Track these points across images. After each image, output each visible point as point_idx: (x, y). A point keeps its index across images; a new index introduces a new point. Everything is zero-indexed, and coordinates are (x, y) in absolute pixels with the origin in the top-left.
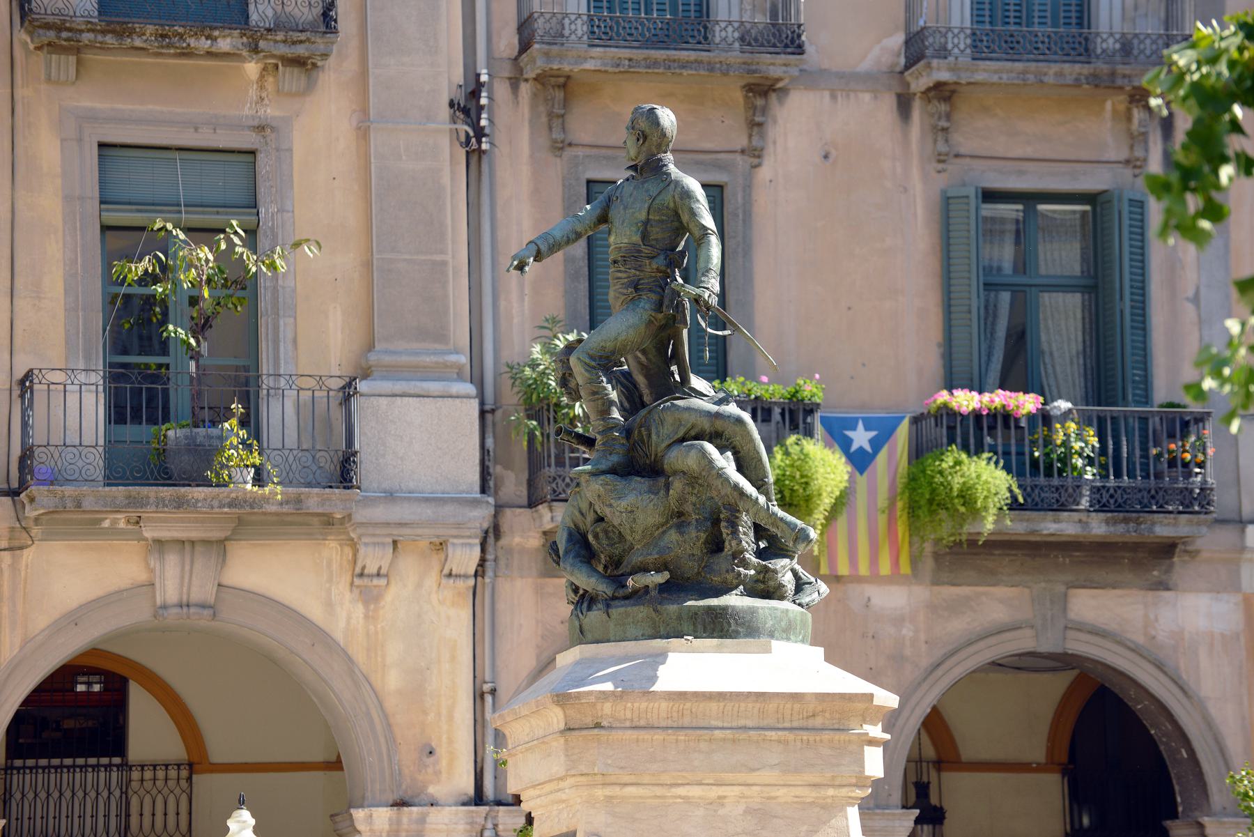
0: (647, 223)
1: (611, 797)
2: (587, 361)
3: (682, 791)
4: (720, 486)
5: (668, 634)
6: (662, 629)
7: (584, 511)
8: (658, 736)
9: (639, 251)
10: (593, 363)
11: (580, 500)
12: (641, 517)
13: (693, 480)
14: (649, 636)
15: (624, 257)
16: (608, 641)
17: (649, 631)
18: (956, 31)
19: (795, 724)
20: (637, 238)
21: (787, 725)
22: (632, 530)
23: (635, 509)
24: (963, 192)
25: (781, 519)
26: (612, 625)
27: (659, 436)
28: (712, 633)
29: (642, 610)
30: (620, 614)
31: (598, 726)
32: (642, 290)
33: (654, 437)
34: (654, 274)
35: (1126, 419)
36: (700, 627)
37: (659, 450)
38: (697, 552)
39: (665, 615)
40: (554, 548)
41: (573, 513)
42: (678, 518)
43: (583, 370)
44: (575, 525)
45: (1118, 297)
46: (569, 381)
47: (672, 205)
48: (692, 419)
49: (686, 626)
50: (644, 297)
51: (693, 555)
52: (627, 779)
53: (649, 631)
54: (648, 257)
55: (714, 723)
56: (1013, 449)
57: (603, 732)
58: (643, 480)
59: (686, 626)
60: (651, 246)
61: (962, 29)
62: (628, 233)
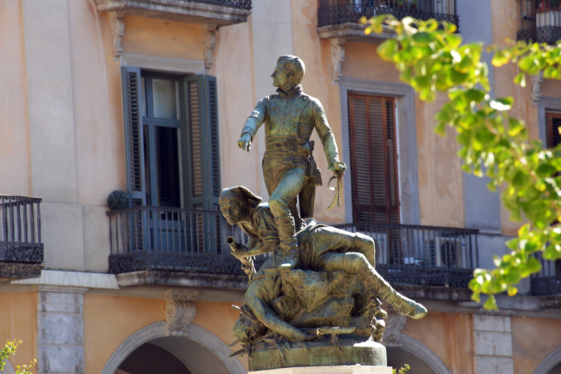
0: (299, 124)
2: (283, 203)
4: (372, 279)
5: (346, 363)
6: (343, 360)
7: (268, 289)
9: (296, 140)
10: (286, 205)
11: (265, 283)
12: (318, 295)
14: (335, 363)
15: (285, 143)
16: (308, 366)
17: (336, 361)
20: (294, 133)
23: (315, 290)
25: (403, 299)
26: (311, 357)
27: (316, 248)
28: (367, 363)
29: (331, 348)
30: (317, 350)
32: (298, 162)
33: (314, 248)
34: (302, 154)
36: (362, 359)
37: (317, 255)
39: (345, 352)
40: (117, 297)
41: (260, 289)
42: (333, 296)
43: (281, 209)
44: (263, 297)
46: (233, 212)
47: (311, 115)
48: (340, 239)
49: (356, 359)
50: (300, 167)
51: (346, 317)
53: (336, 361)
54: (299, 144)
56: (179, 229)
58: (316, 273)
59: (356, 359)
60: (301, 138)
62: (289, 129)
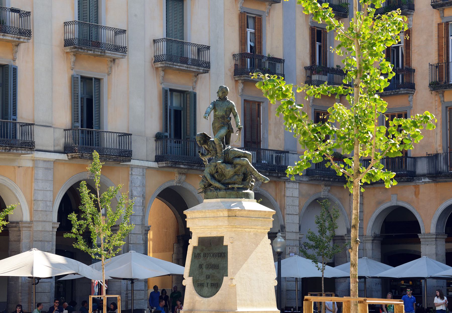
0: (226, 110)
1: (235, 230)
3: (246, 230)
8: (244, 218)
13: (242, 166)
18: (13, 28)
19: (263, 217)
20: (224, 114)
21: (262, 217)
22: (228, 175)
24: (77, 76)
31: (236, 216)
35: (93, 132)
36: (245, 196)
37: (231, 159)
38: (241, 181)
42: (236, 174)
45: (10, 90)
48: (239, 153)
49: (243, 196)
52: (239, 227)
55: (252, 216)
57: (236, 217)
59: (243, 196)
61: (77, 38)
